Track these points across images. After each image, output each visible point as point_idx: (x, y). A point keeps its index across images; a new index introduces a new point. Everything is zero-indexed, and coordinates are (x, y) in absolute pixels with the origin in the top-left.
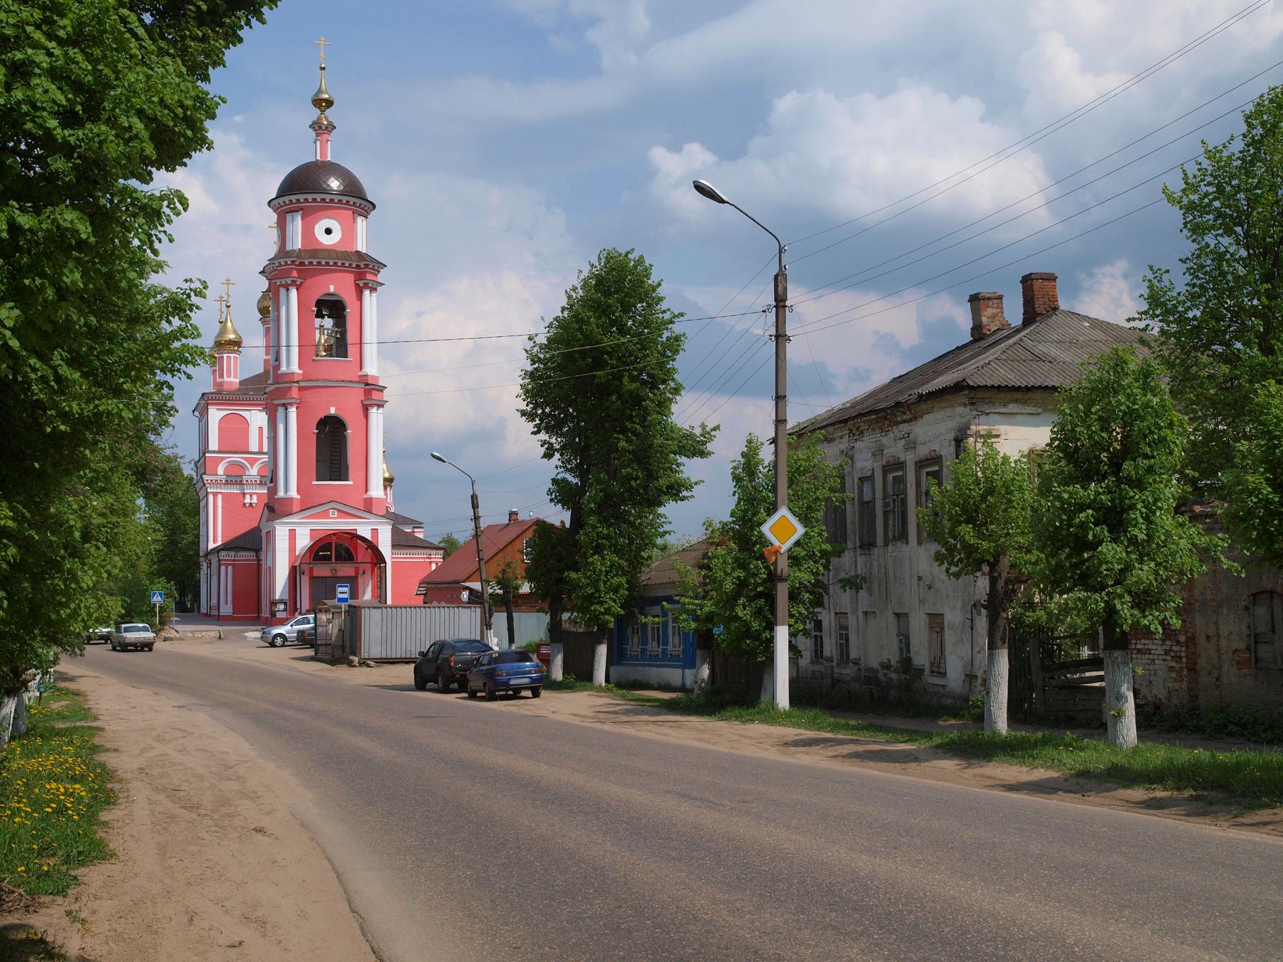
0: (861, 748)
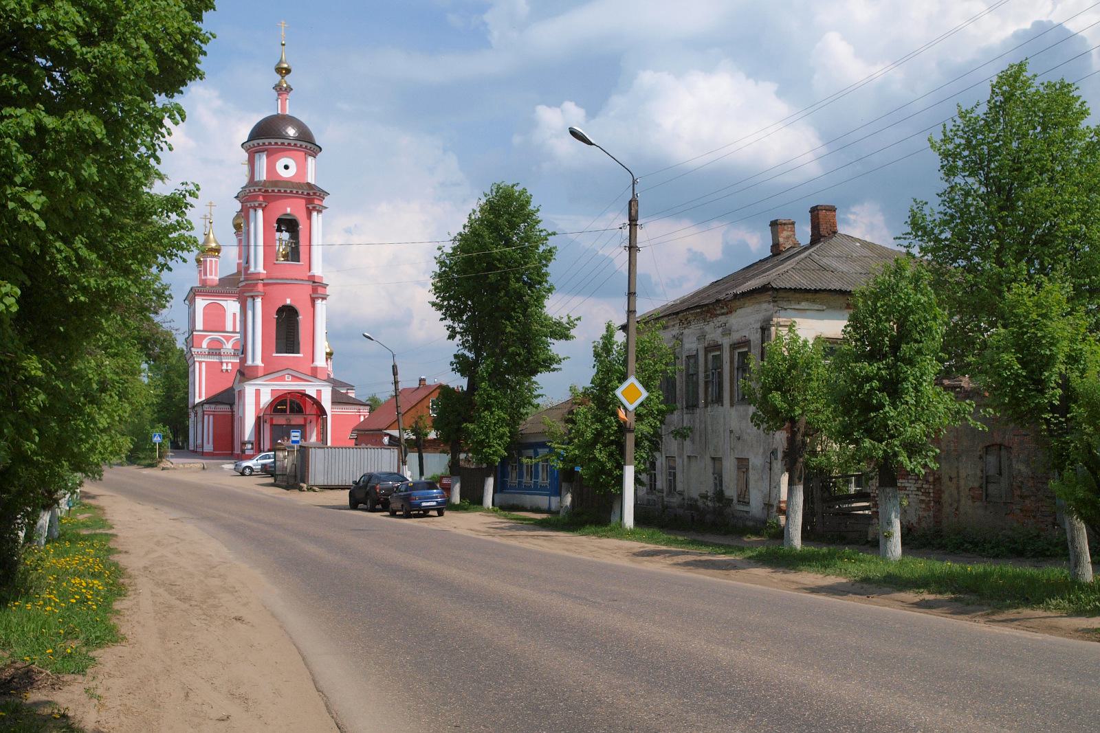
0: (690, 558)
